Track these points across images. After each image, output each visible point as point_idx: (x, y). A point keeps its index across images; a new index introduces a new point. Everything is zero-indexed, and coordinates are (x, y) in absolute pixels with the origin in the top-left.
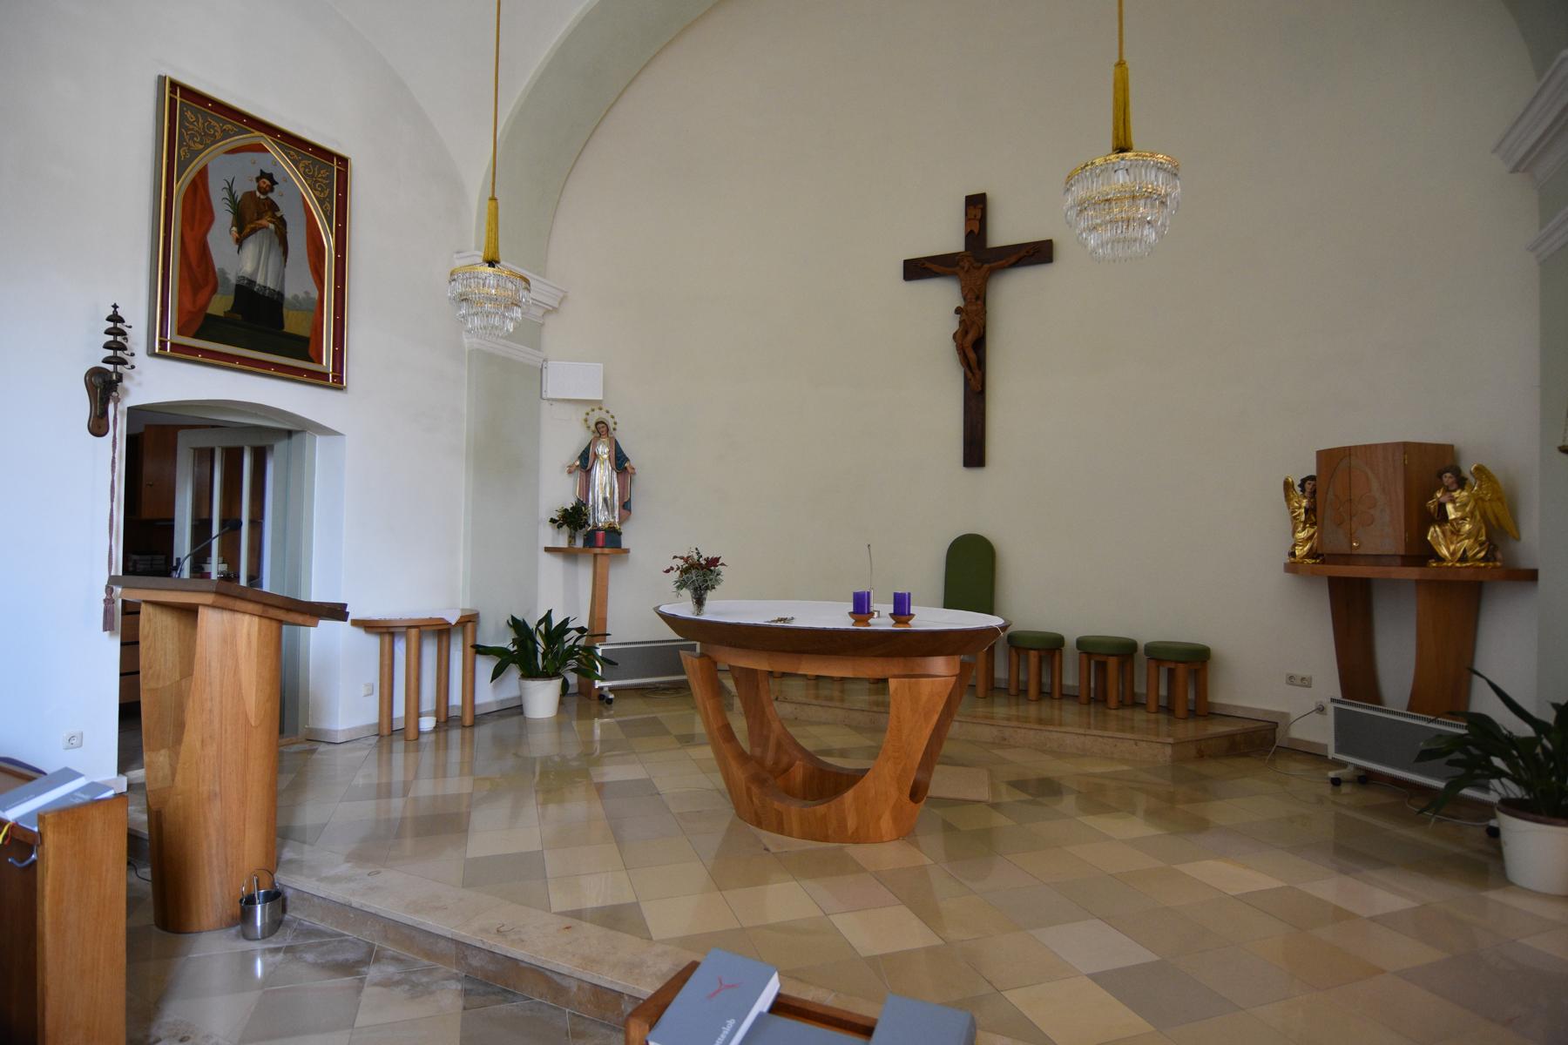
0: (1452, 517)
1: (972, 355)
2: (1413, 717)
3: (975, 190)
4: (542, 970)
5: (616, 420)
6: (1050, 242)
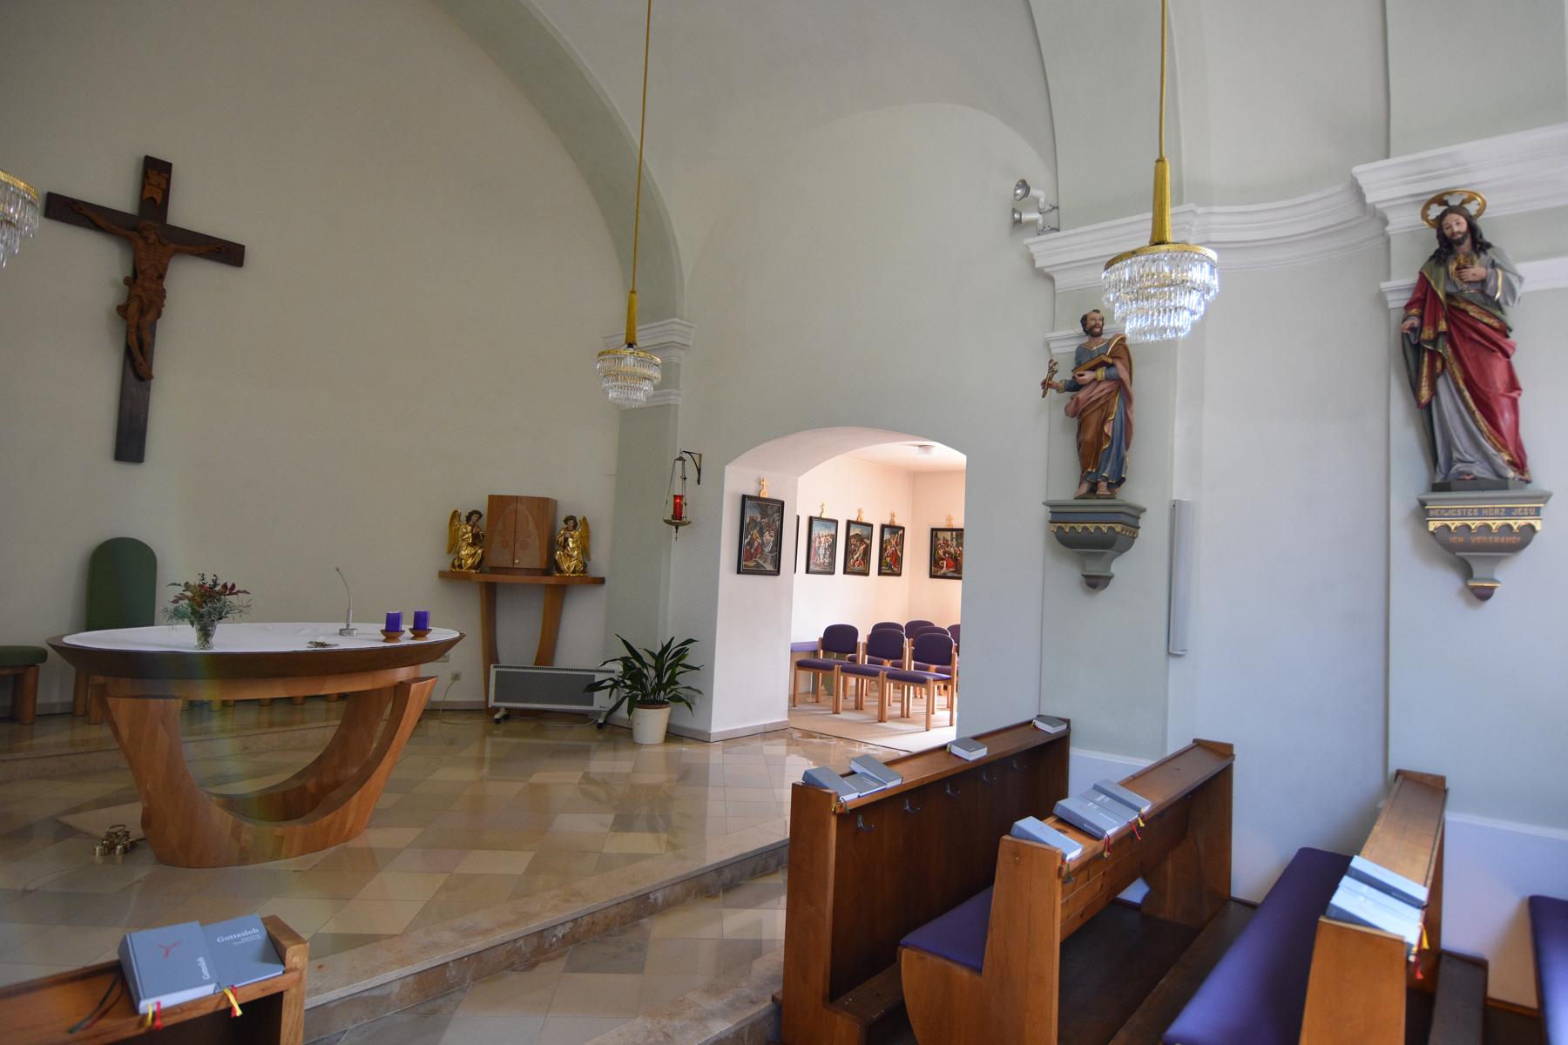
2: (537, 669)
4: (358, 995)
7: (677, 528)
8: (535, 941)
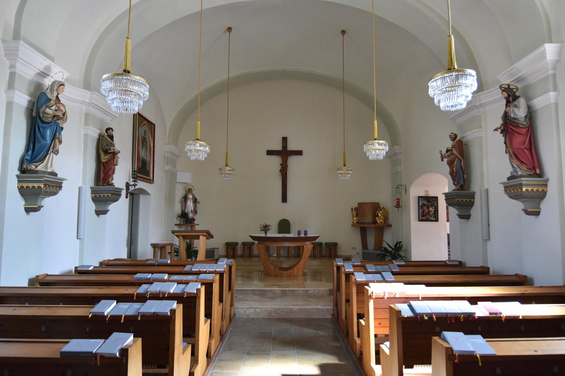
0: (379, 216)
5: (194, 188)
6: (302, 151)
7: (398, 208)
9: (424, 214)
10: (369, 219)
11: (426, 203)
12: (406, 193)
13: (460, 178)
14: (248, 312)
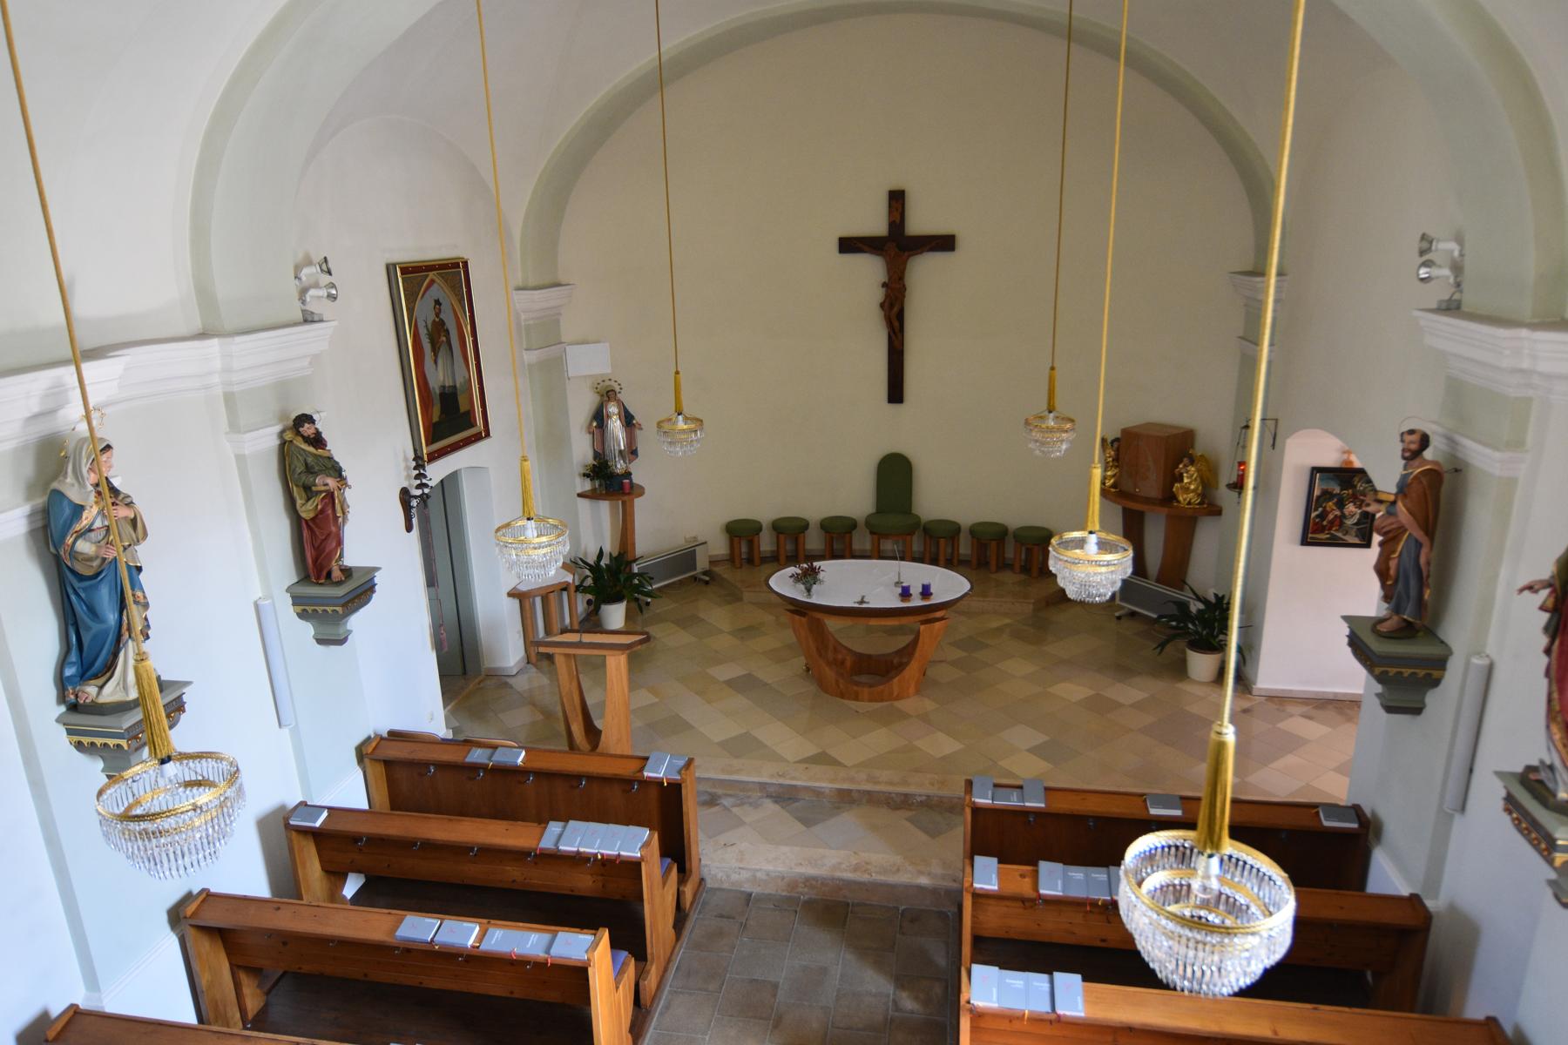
1: (896, 324)
3: (896, 186)
8: (903, 798)
9: (1325, 523)
10: (1150, 487)
11: (1337, 490)
12: (1273, 445)
13: (1408, 597)
14: (735, 877)
